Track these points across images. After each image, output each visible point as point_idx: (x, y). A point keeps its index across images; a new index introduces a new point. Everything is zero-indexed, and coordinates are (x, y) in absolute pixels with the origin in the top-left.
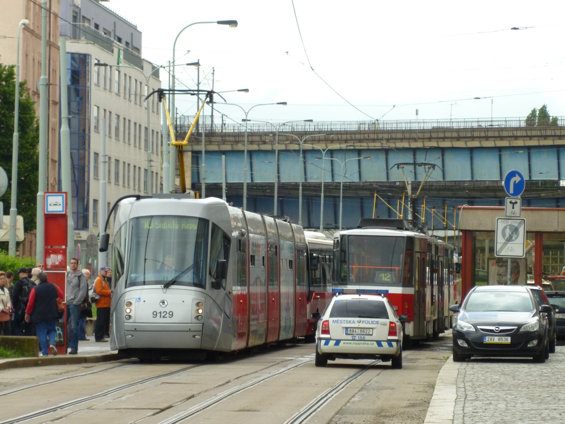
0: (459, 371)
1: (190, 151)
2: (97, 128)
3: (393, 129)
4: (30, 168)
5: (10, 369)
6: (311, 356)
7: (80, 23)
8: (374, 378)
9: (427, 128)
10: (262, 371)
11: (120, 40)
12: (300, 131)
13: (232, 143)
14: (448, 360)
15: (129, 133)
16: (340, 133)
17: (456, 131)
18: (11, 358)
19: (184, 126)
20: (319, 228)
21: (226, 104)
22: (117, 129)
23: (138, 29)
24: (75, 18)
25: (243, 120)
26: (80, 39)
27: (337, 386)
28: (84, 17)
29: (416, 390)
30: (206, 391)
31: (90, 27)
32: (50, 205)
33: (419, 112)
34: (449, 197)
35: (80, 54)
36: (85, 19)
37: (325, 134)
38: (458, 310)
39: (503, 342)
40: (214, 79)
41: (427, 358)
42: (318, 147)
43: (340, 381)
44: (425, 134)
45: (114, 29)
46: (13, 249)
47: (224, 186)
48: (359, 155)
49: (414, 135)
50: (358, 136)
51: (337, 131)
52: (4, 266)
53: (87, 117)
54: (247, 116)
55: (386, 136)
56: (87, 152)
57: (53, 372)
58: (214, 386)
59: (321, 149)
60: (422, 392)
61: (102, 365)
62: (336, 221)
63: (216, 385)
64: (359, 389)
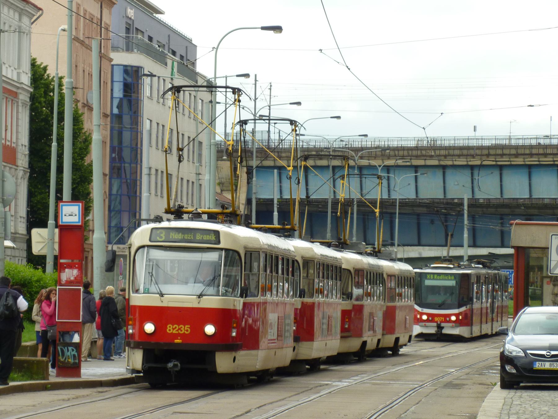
4: (79, 180)
5: (15, 394)
6: (349, 381)
7: (133, 35)
8: (411, 408)
9: (485, 145)
10: (291, 398)
11: (174, 53)
12: (357, 147)
14: (495, 387)
17: (514, 147)
18: (17, 381)
20: (394, 245)
23: (193, 42)
24: (128, 30)
26: (132, 51)
28: (137, 29)
31: (143, 40)
32: (65, 215)
33: (477, 129)
35: (132, 67)
38: (507, 333)
39: (555, 367)
40: (271, 95)
41: (474, 383)
42: (374, 163)
43: (372, 411)
45: (168, 42)
46: (50, 263)
49: (472, 152)
50: (415, 153)
52: (30, 281)
53: (139, 130)
56: (139, 166)
57: (61, 397)
59: (377, 165)
61: (119, 389)
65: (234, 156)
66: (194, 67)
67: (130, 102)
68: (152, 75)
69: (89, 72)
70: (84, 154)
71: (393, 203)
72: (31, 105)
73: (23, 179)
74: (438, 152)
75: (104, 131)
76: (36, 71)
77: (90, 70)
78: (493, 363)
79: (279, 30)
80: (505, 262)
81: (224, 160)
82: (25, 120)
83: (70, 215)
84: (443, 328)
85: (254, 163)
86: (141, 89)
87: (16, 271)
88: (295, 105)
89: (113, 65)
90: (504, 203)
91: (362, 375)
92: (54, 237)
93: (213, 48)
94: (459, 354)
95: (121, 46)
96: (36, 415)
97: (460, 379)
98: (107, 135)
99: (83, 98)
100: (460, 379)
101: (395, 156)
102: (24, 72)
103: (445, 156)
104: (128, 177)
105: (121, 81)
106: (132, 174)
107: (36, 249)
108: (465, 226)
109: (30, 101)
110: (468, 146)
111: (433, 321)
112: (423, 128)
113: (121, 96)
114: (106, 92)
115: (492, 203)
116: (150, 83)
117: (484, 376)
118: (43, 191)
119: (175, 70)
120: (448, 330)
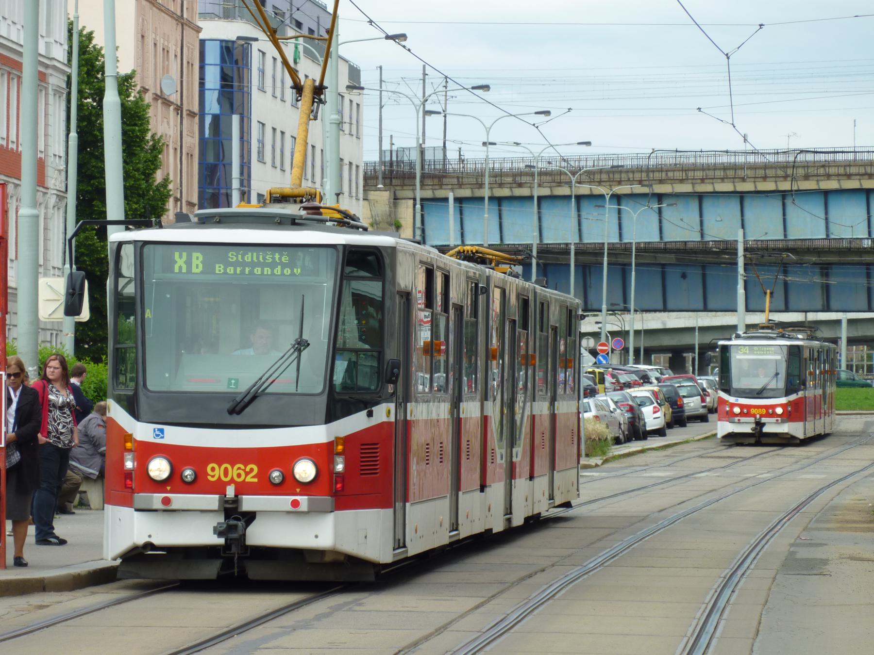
1: (410, 199)
2: (261, 153)
13: (472, 186)
20: (600, 311)
45: (289, 8)
49: (740, 173)
50: (657, 175)
55: (699, 174)
62: (625, 300)
65: (393, 184)
70: (151, 169)
71: (626, 249)
73: (56, 208)
75: (190, 138)
81: (379, 190)
82: (59, 115)
84: (764, 424)
89: (202, 42)
98: (194, 144)
99: (155, 86)
101: (629, 180)
102: (56, 41)
108: (739, 277)
112: (727, 55)
114: (192, 81)
118: (88, 226)
120: (771, 427)
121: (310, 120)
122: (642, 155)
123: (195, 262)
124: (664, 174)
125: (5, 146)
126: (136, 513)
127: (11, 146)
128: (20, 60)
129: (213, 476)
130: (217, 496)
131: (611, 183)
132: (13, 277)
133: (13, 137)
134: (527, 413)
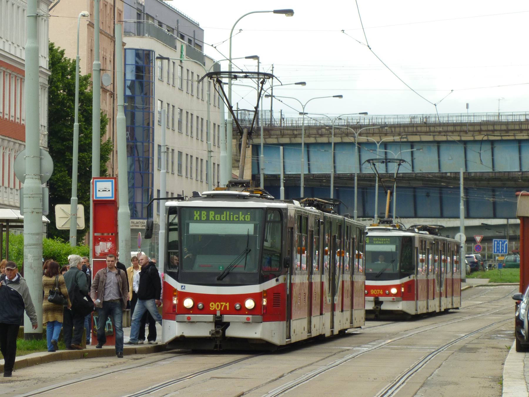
0: (524, 363)
3: (445, 122)
5: (54, 362)
6: (368, 346)
7: (144, 20)
8: (435, 371)
11: (182, 37)
13: (290, 136)
14: (510, 350)
15: (192, 127)
16: (393, 126)
19: (245, 120)
20: (374, 217)
21: (282, 85)
22: (180, 122)
23: (200, 26)
24: (139, 16)
25: (301, 113)
26: (144, 35)
27: (397, 380)
29: (482, 385)
30: (257, 388)
32: (99, 191)
33: (470, 106)
34: (498, 187)
35: (144, 50)
36: (149, 18)
37: (379, 127)
38: (522, 298)
41: (487, 347)
43: (399, 375)
44: (475, 127)
47: (282, 177)
48: (412, 147)
49: (464, 128)
50: (410, 129)
51: (391, 124)
53: (151, 111)
54: (304, 109)
56: (151, 145)
57: (99, 364)
58: (266, 382)
60: (488, 387)
63: (269, 380)
64: (421, 384)
66: (201, 50)
67: (141, 84)
68: (161, 58)
69: (103, 56)
72: (50, 88)
74: (445, 128)
76: (54, 55)
77: (105, 54)
78: (498, 328)
79: (290, 14)
80: (497, 232)
82: (44, 101)
83: (103, 191)
85: (261, 141)
86: (153, 72)
87: (45, 244)
88: (300, 85)
89: (125, 49)
90: (495, 176)
91: (379, 341)
92: (77, 212)
93: (240, 30)
94: (464, 319)
95: (133, 31)
96: (80, 382)
97: (473, 343)
100: (473, 343)
103: (452, 132)
104: (140, 155)
105: (132, 64)
106: (145, 152)
107: (60, 224)
108: (461, 198)
109: (49, 84)
110: (461, 123)
111: (205, 311)
113: (134, 78)
115: (485, 176)
116: (160, 66)
117: (494, 340)
119: (184, 53)
121: (247, 147)
122: (401, 116)
123: (203, 215)
124: (415, 129)
125: (14, 121)
126: (177, 323)
127: (17, 121)
128: (23, 69)
129: (212, 308)
130: (213, 315)
131: (381, 135)
132: (6, 198)
133: (18, 115)
134: (341, 280)
